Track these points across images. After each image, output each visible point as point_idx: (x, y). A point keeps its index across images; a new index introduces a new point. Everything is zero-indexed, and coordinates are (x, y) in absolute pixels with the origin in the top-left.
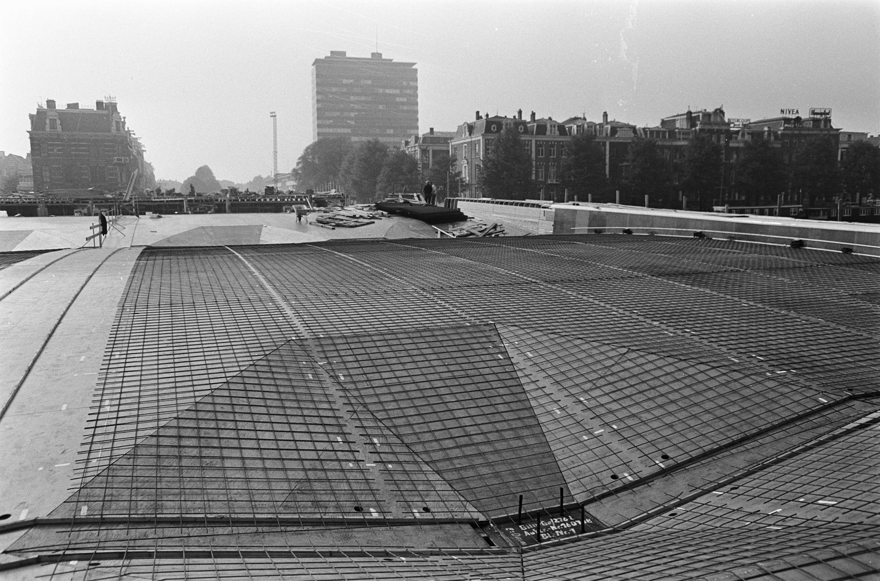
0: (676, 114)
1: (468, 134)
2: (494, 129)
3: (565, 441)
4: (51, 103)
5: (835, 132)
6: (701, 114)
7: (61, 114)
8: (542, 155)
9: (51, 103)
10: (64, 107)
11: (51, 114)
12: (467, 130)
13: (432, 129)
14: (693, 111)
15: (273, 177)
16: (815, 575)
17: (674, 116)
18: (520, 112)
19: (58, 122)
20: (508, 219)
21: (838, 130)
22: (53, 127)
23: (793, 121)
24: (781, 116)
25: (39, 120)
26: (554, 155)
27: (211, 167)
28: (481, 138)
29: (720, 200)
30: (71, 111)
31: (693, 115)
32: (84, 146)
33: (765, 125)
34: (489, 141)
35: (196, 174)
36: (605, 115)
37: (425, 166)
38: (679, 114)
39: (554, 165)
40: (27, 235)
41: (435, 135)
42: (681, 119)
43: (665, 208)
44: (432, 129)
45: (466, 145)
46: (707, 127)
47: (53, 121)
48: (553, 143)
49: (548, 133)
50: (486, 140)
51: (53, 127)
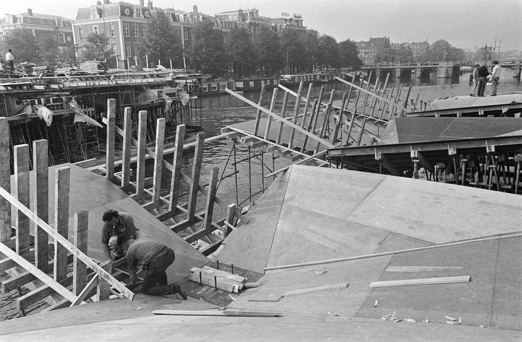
0: (224, 11)
1: (98, 16)
2: (128, 13)
3: (253, 163)
5: (304, 29)
6: (248, 12)
8: (128, 35)
12: (97, 13)
14: (243, 9)
16: (490, 201)
17: (223, 13)
21: (306, 28)
23: (289, 21)
24: (281, 16)
26: (128, 35)
28: (119, 20)
31: (243, 12)
33: (273, 22)
34: (125, 24)
36: (195, 7)
37: (188, 43)
38: (226, 11)
39: (129, 43)
41: (34, 16)
42: (233, 15)
45: (97, 26)
46: (253, 21)
49: (135, 15)
50: (123, 22)
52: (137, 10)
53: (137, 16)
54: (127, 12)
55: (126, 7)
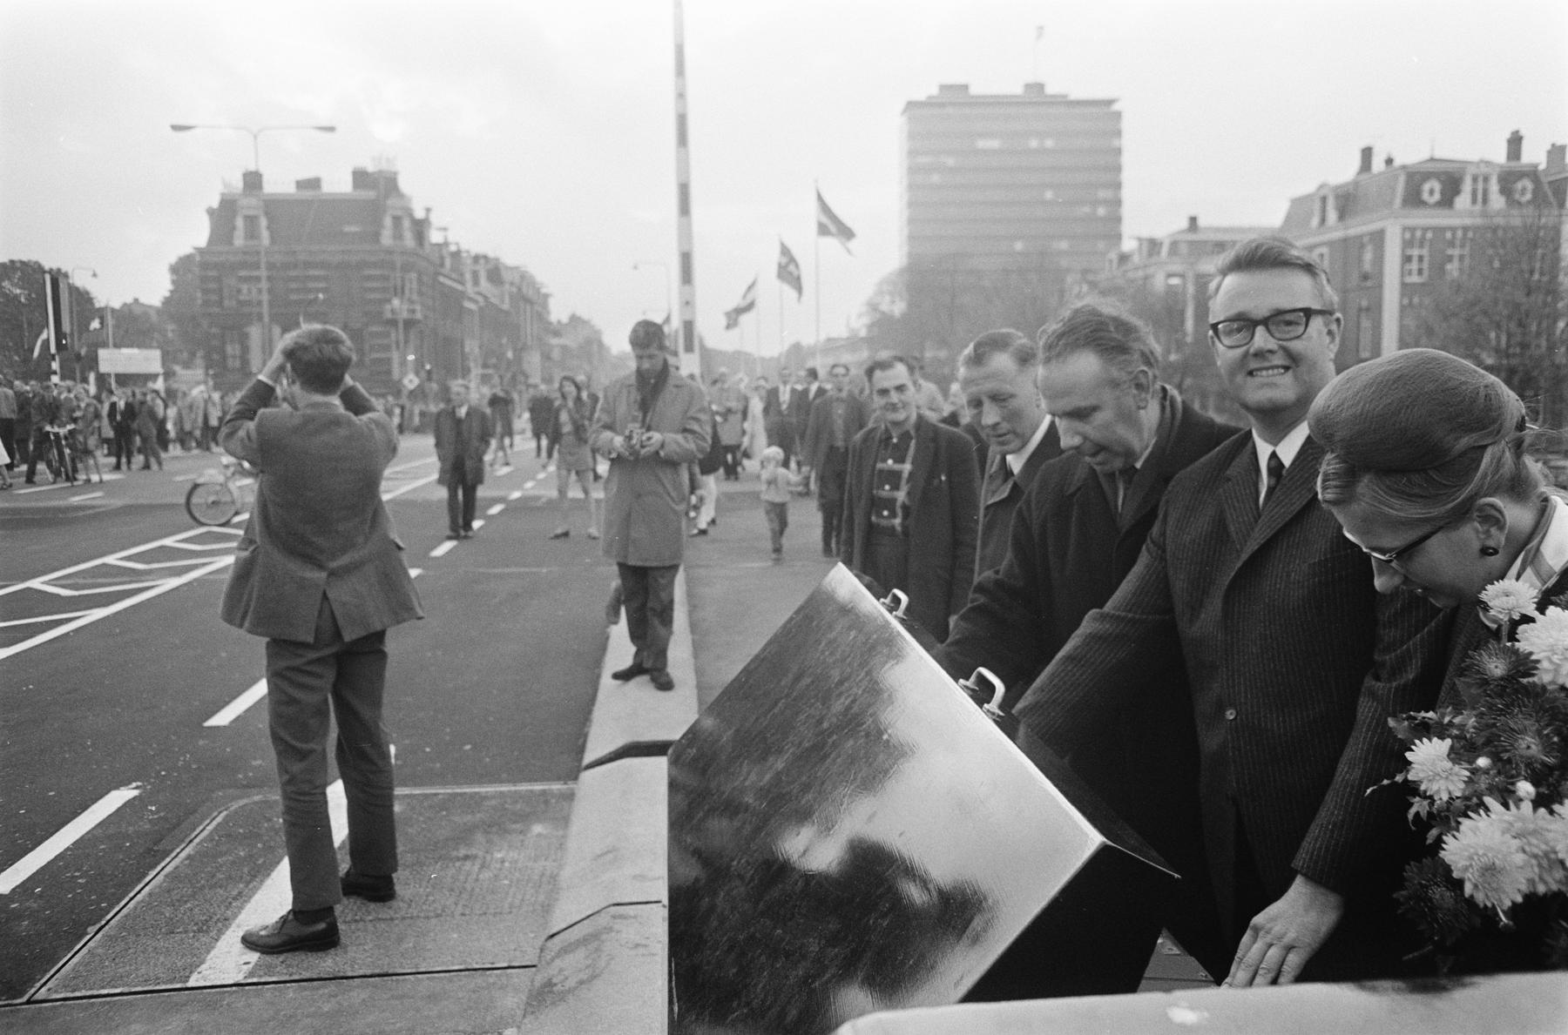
4: (253, 181)
7: (274, 206)
9: (253, 181)
10: (289, 188)
11: (250, 204)
13: (1193, 220)
15: (1482, 406)
18: (1515, 142)
19: (263, 222)
20: (250, 594)
22: (252, 233)
25: (174, 269)
27: (173, 259)
29: (510, 899)
30: (308, 194)
32: (317, 279)
35: (163, 303)
40: (1225, 528)
43: (291, 870)
44: (1193, 220)
47: (251, 221)
48: (1418, 234)
51: (252, 233)
52: (1475, 179)
53: (1474, 201)
54: (1432, 192)
55: (1427, 176)
